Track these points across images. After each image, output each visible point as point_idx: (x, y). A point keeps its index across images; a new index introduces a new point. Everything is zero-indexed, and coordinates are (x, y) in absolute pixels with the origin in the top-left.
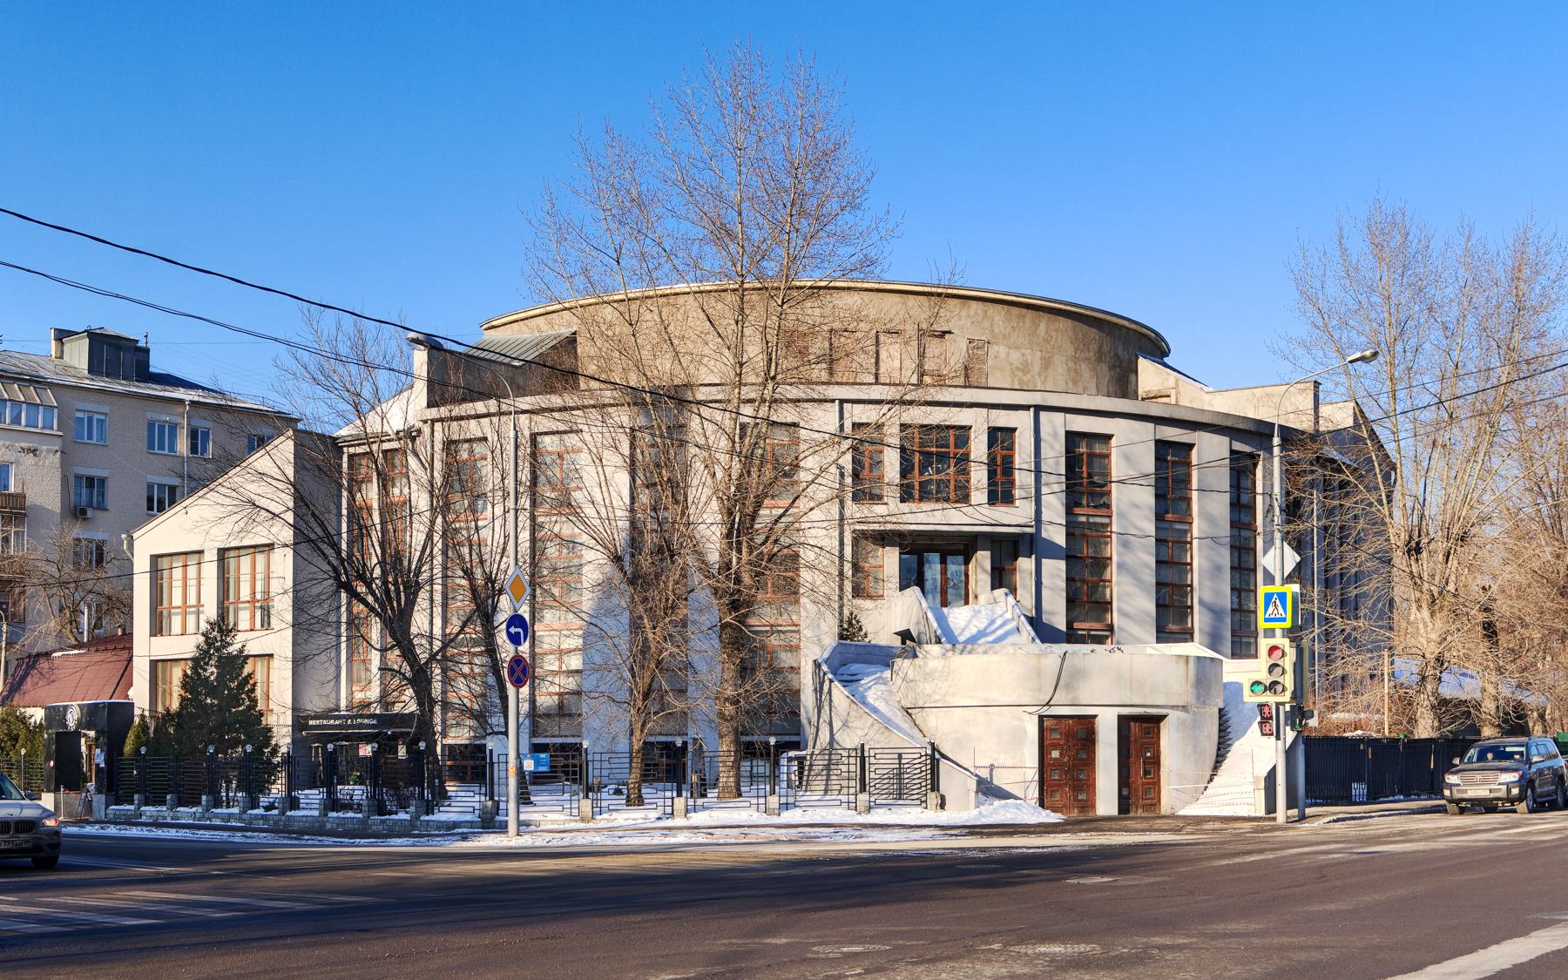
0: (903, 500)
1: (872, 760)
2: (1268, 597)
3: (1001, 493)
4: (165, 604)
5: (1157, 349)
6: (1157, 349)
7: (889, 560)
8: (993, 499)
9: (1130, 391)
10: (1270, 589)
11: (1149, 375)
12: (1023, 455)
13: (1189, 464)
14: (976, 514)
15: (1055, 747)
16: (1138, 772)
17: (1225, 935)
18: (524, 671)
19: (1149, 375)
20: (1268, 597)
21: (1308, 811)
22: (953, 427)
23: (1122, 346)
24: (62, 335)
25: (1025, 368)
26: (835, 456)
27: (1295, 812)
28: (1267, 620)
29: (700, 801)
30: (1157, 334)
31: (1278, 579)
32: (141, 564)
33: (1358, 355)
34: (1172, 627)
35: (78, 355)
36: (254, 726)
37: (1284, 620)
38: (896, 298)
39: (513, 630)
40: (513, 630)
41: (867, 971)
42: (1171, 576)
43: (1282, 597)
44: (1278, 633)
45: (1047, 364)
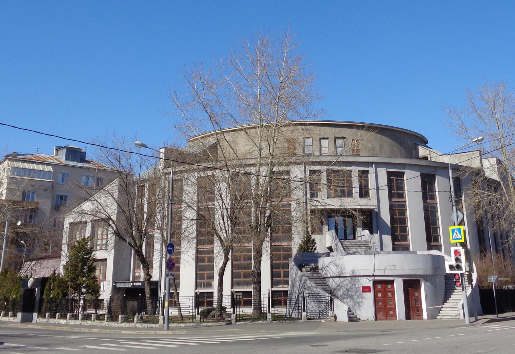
0: (288, 284)
1: (191, 305)
2: (453, 231)
3: (364, 193)
4: (95, 239)
5: (424, 142)
6: (424, 142)
7: (433, 243)
8: (361, 196)
9: (414, 154)
10: (454, 227)
11: (422, 151)
12: (372, 184)
13: (403, 180)
14: (354, 202)
15: (379, 292)
16: (412, 303)
17: (317, 346)
18: (173, 265)
19: (422, 151)
20: (453, 231)
21: (479, 317)
22: (351, 254)
23: (408, 141)
24: (58, 149)
25: (374, 149)
26: (113, 218)
27: (473, 319)
28: (453, 239)
29: (205, 320)
30: (422, 136)
31: (456, 223)
32: (66, 225)
33: (476, 139)
34: (433, 243)
35: (63, 154)
36: (494, 181)
37: (461, 239)
38: (365, 278)
39: (169, 248)
40: (169, 248)
41: (226, 324)
42: (284, 173)
43: (459, 230)
44: (458, 244)
45: (381, 147)
